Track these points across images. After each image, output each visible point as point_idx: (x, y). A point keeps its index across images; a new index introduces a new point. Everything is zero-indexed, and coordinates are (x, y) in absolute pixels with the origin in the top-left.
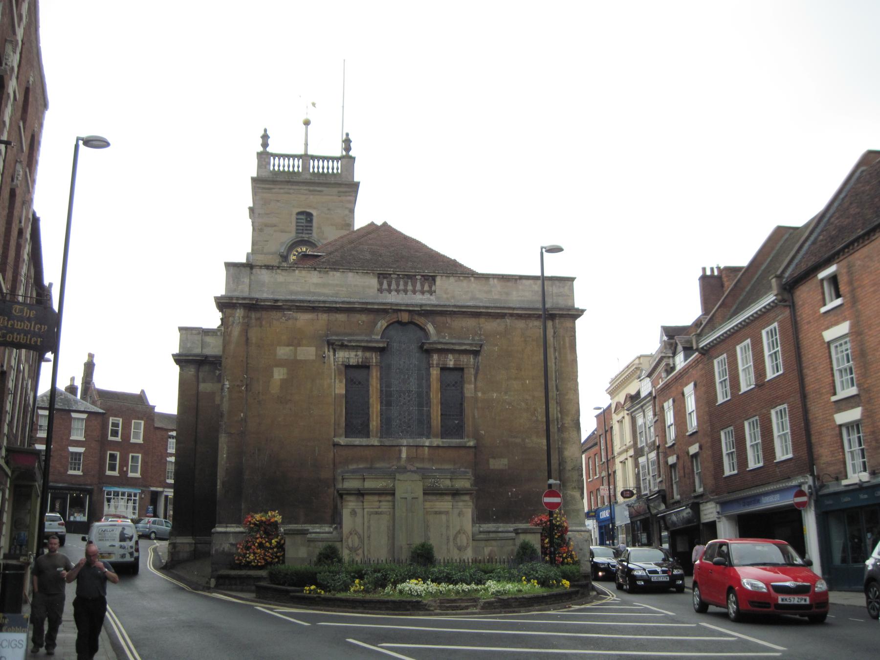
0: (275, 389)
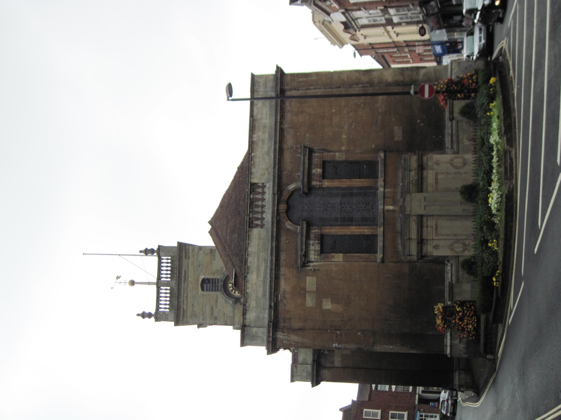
0: (339, 308)
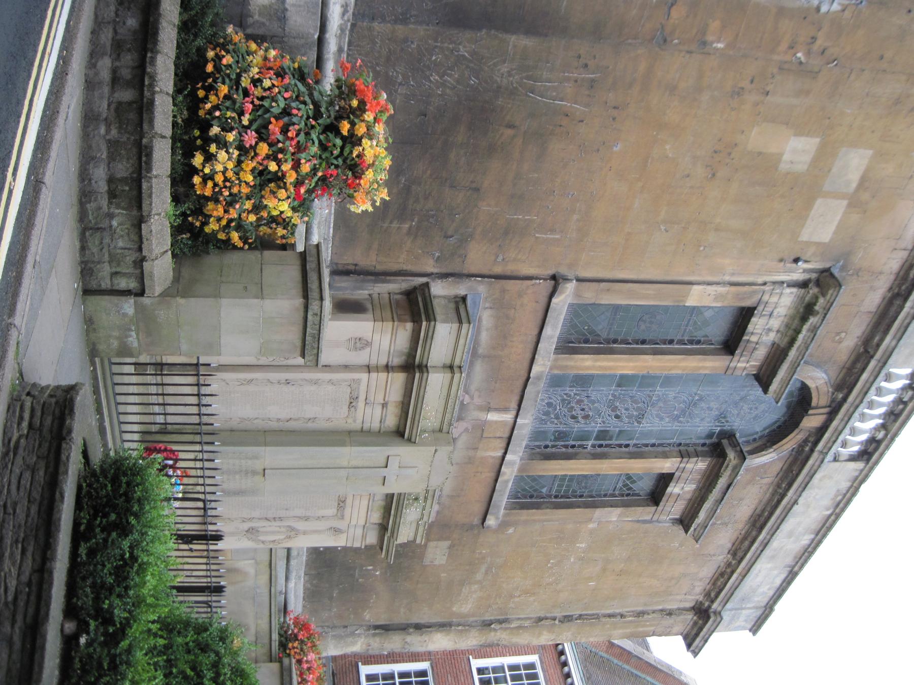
0: (758, 138)
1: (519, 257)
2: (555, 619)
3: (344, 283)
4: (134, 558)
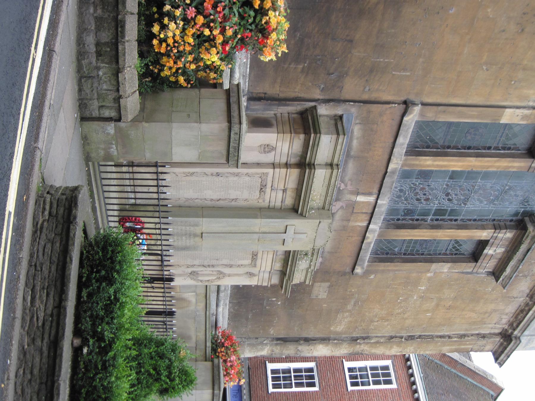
1: (381, 88)
2: (402, 337)
3: (257, 106)
4: (117, 299)
